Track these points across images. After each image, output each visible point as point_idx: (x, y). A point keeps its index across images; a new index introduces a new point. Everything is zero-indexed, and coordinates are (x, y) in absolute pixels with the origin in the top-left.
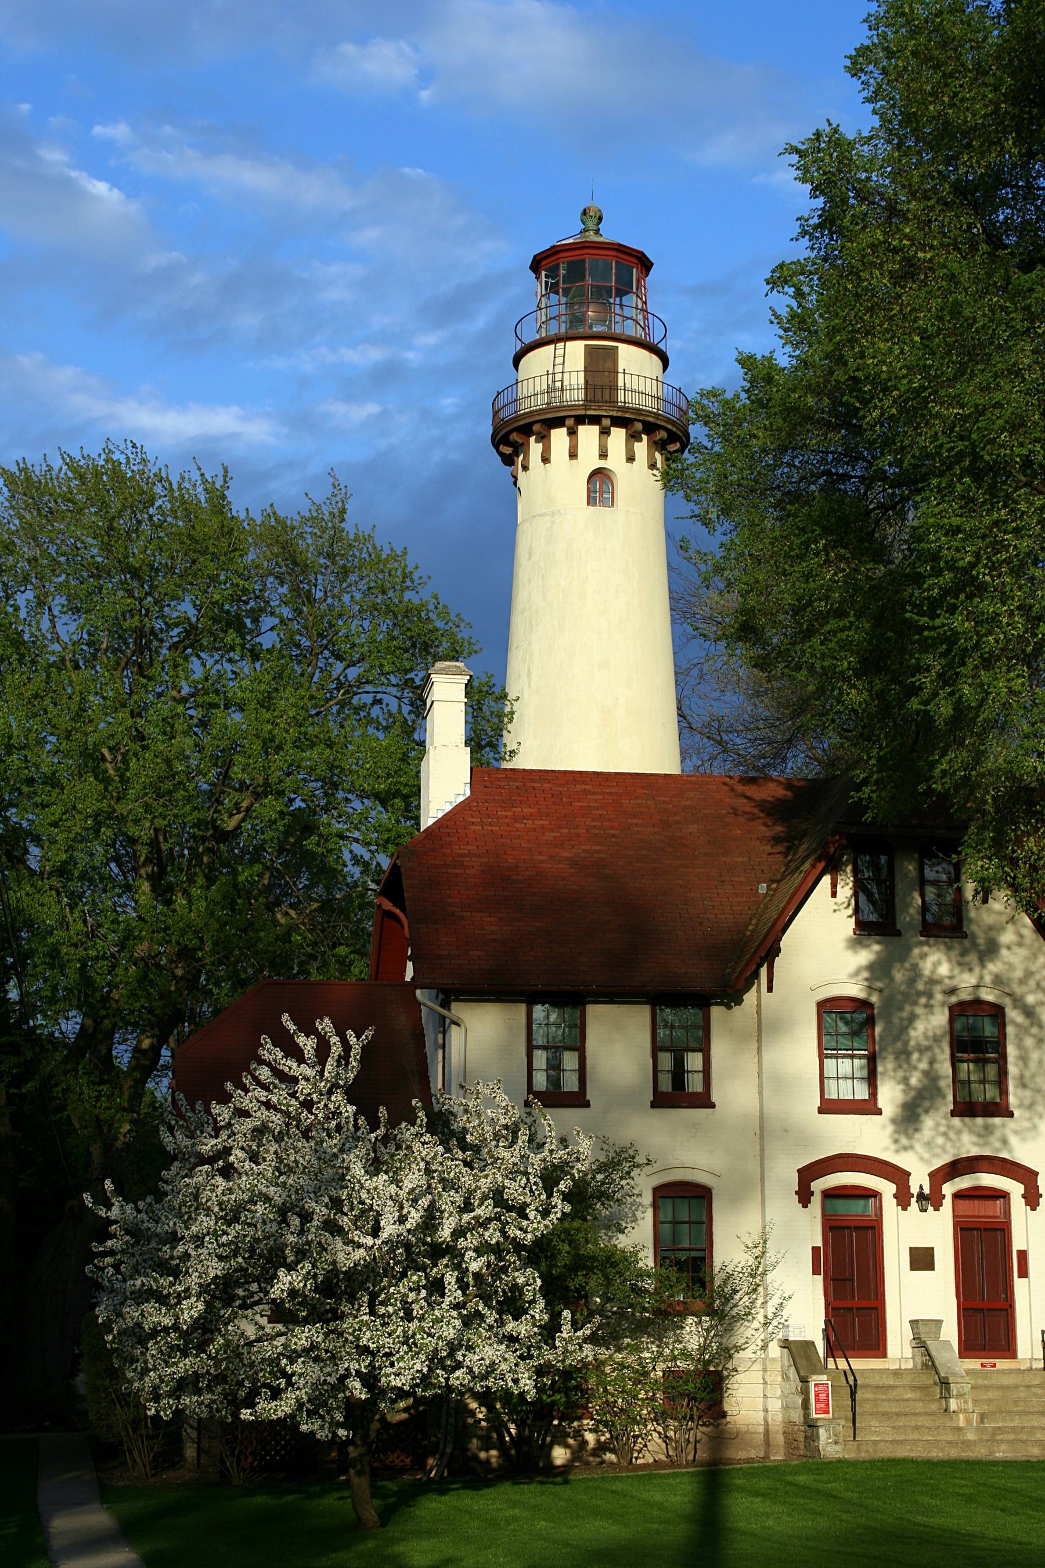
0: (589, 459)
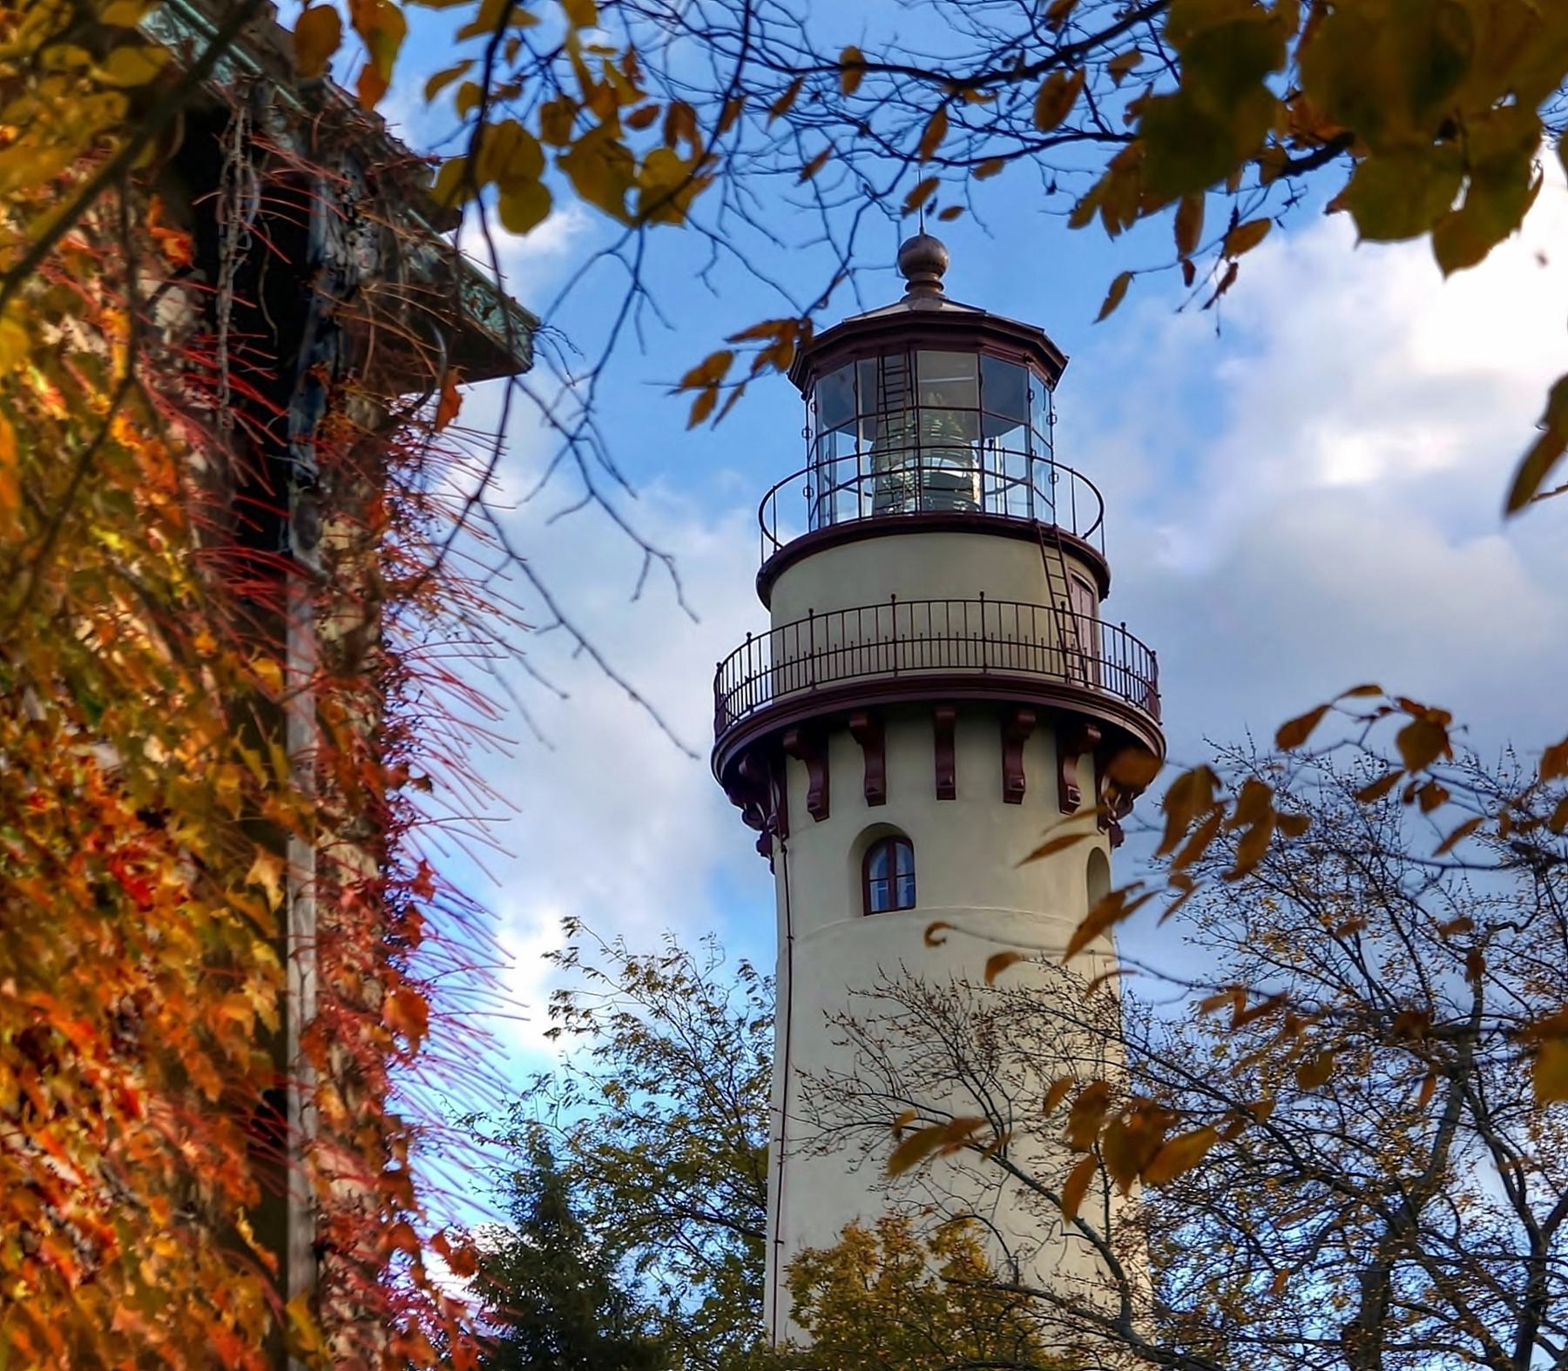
0: (851, 815)
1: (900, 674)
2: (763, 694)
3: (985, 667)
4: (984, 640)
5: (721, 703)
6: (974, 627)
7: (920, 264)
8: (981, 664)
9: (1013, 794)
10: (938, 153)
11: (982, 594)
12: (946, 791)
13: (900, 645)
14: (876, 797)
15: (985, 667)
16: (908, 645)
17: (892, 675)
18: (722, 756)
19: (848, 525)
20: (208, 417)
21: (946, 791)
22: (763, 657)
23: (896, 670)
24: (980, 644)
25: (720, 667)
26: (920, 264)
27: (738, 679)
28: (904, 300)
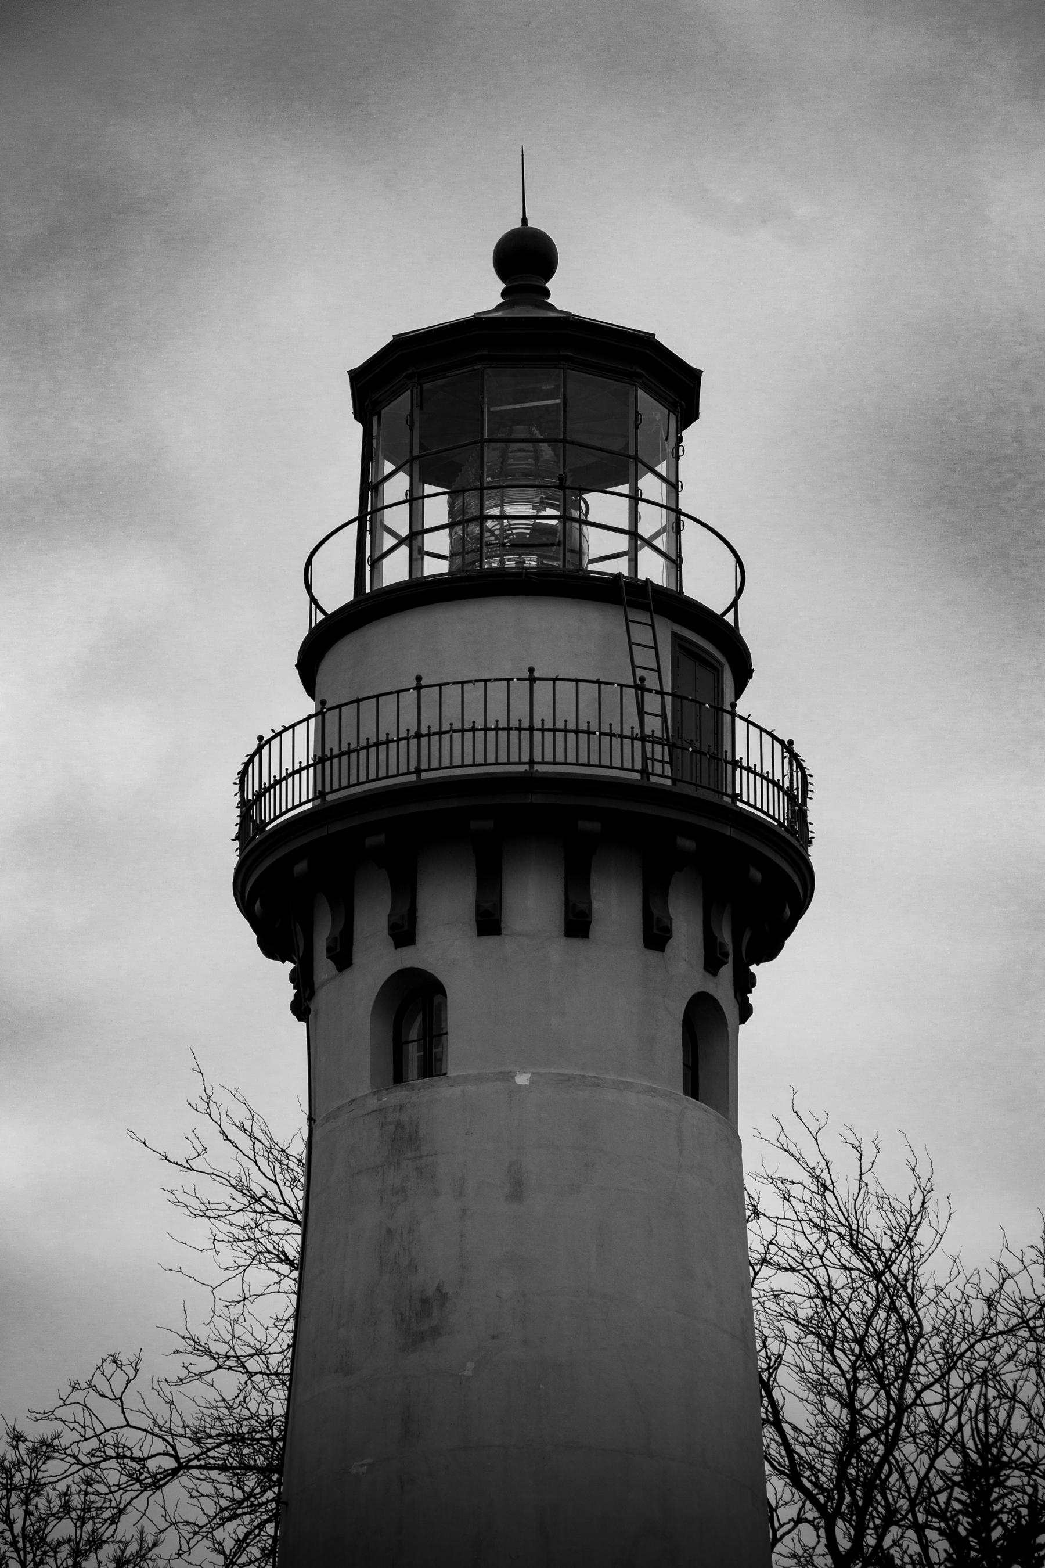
0: (377, 961)
1: (425, 776)
2: (297, 797)
3: (531, 762)
4: (531, 729)
5: (246, 807)
6: (520, 712)
7: (525, 258)
8: (526, 758)
9: (577, 924)
10: (356, 523)
11: (531, 670)
12: (489, 923)
13: (424, 740)
14: (403, 933)
15: (531, 762)
16: (457, 736)
17: (413, 777)
18: (242, 893)
19: (397, 588)
20: (918, 1402)
21: (489, 923)
22: (301, 747)
23: (418, 771)
24: (526, 734)
25: (262, 743)
26: (525, 258)
27: (275, 772)
28: (500, 307)
